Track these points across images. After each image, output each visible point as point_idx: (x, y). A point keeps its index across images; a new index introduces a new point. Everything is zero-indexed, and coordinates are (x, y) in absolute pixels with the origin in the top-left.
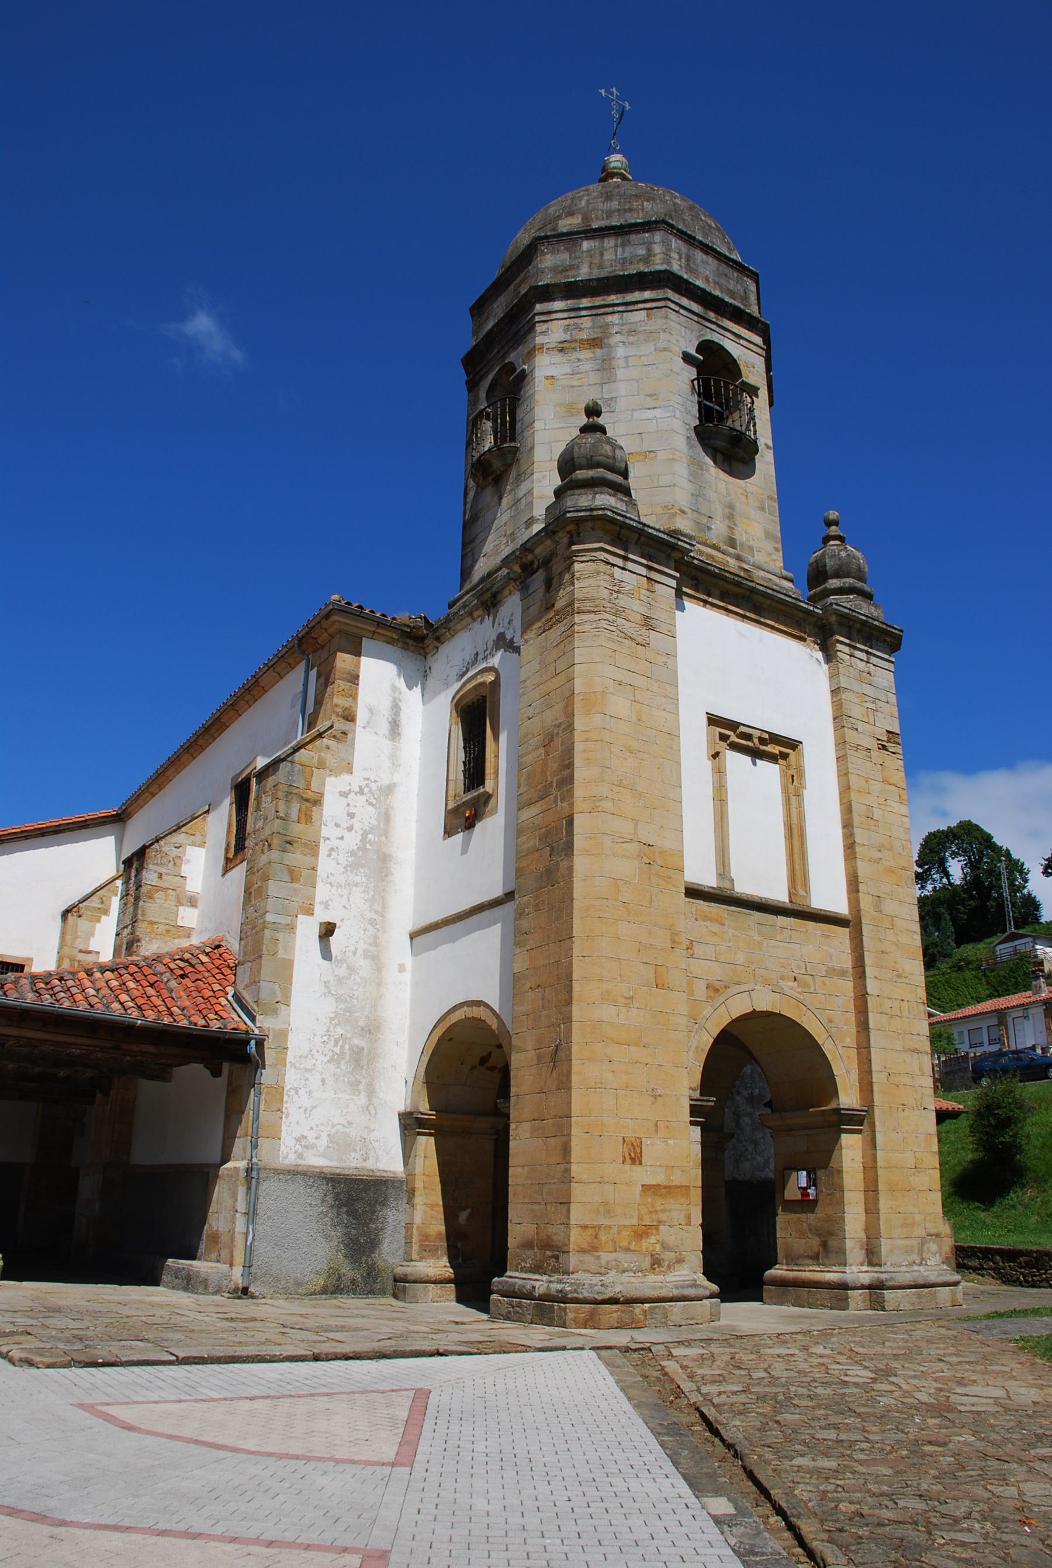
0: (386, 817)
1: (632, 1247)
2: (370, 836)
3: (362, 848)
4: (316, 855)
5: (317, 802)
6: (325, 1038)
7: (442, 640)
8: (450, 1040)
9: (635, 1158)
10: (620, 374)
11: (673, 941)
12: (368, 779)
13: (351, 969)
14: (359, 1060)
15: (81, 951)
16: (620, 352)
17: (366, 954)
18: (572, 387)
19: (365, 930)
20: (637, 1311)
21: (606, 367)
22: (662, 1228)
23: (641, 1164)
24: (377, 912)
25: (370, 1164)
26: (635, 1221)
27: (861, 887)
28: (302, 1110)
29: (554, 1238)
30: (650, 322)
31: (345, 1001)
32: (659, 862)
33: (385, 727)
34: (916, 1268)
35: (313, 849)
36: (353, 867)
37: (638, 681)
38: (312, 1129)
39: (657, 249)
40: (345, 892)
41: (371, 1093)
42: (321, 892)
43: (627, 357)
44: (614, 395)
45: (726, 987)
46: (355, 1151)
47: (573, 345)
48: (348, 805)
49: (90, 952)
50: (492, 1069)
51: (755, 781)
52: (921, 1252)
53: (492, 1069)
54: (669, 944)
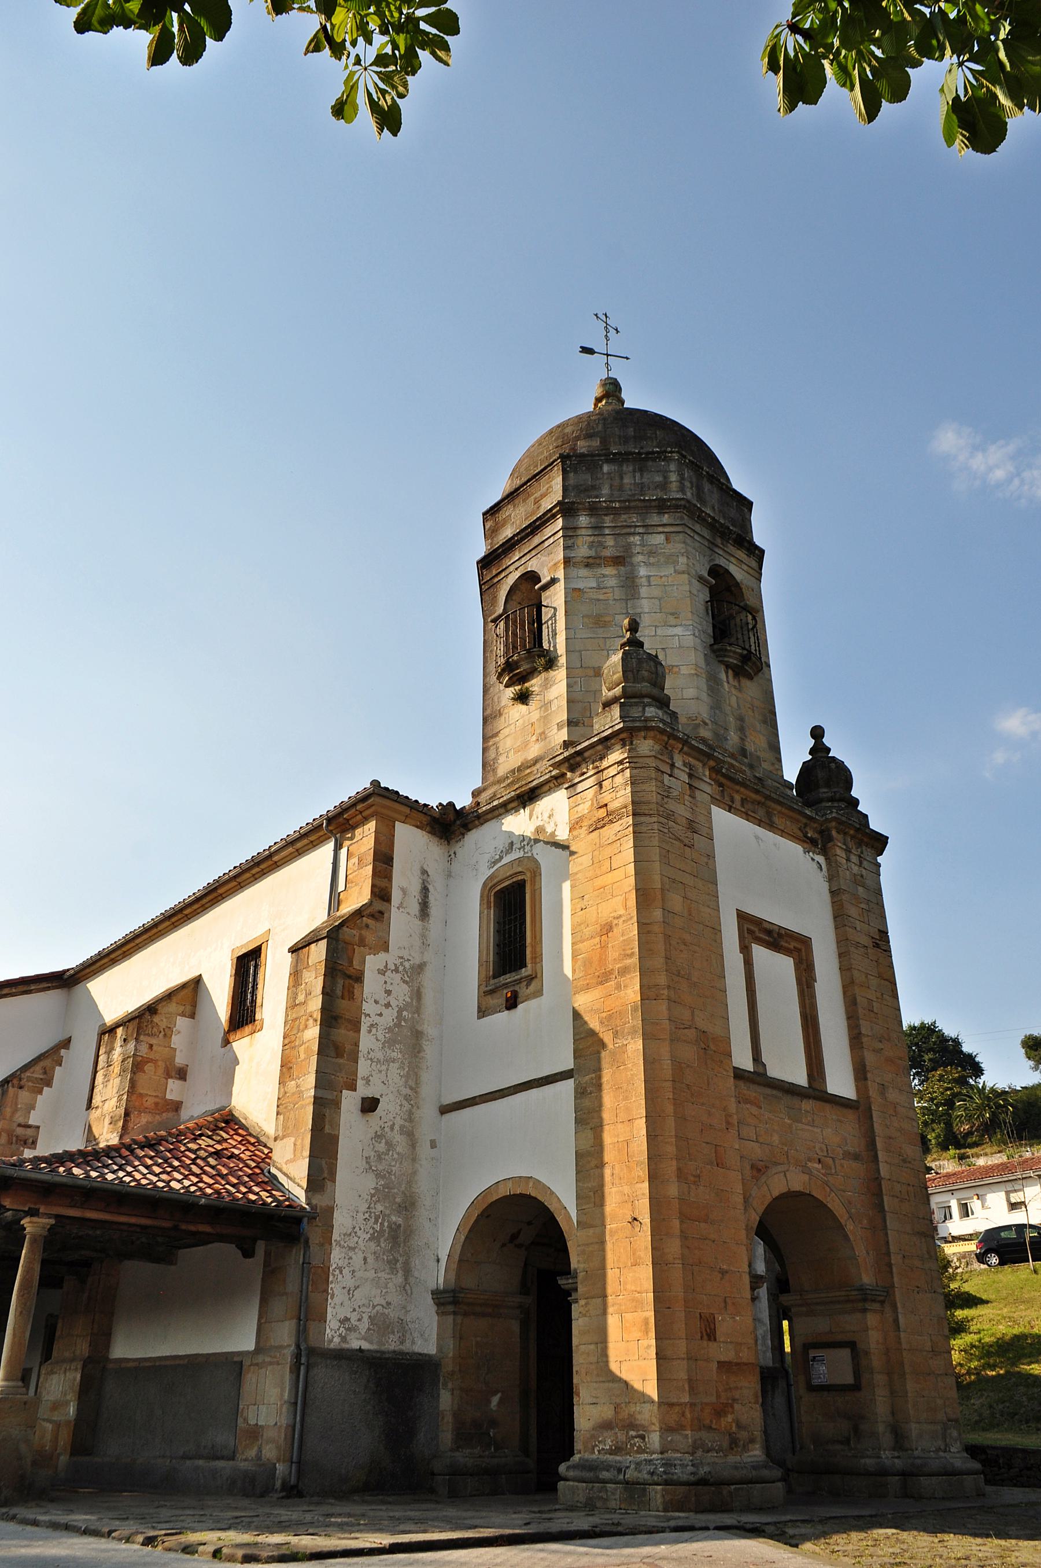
0: (418, 994)
1: (714, 1426)
2: (405, 1013)
3: (398, 1025)
4: (358, 1030)
5: (359, 978)
6: (367, 1215)
7: (470, 826)
8: (488, 1217)
9: (710, 1335)
10: (644, 591)
11: (728, 1123)
12: (402, 958)
13: (389, 1145)
14: (397, 1239)
15: (20, 1125)
16: (643, 571)
17: (403, 1131)
18: (599, 600)
19: (401, 1105)
20: (725, 1492)
21: (630, 586)
22: (737, 1406)
23: (715, 1340)
24: (411, 1088)
25: (407, 1347)
26: (713, 1399)
27: (869, 1075)
28: (346, 1290)
29: (638, 1417)
30: (670, 546)
31: (383, 1177)
32: (712, 1047)
33: (415, 908)
34: (941, 1454)
35: (356, 1026)
36: (389, 1043)
37: (689, 880)
38: (354, 1310)
39: (673, 477)
40: (384, 1067)
41: (407, 1272)
42: (363, 1067)
43: (649, 577)
44: (639, 610)
45: (766, 1167)
46: (393, 1333)
47: (598, 561)
48: (386, 982)
49: (30, 1126)
50: (520, 1246)
51: (775, 968)
52: (944, 1438)
53: (520, 1246)
54: (724, 1126)
